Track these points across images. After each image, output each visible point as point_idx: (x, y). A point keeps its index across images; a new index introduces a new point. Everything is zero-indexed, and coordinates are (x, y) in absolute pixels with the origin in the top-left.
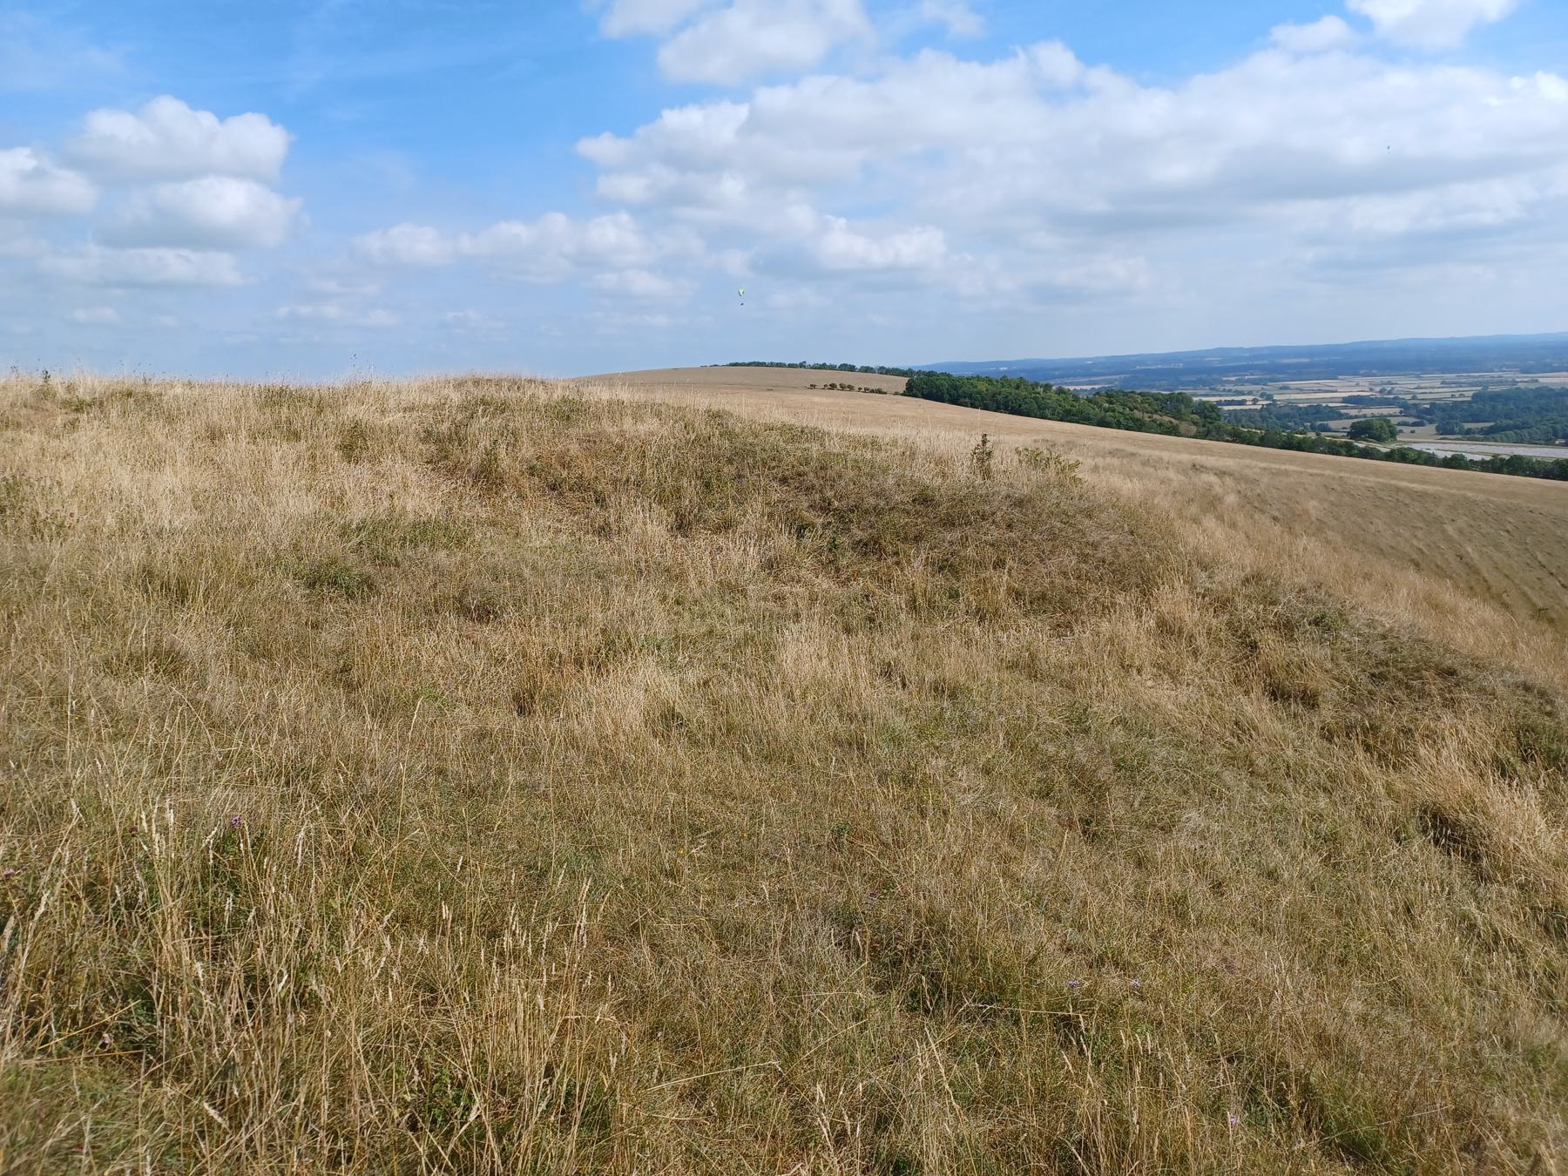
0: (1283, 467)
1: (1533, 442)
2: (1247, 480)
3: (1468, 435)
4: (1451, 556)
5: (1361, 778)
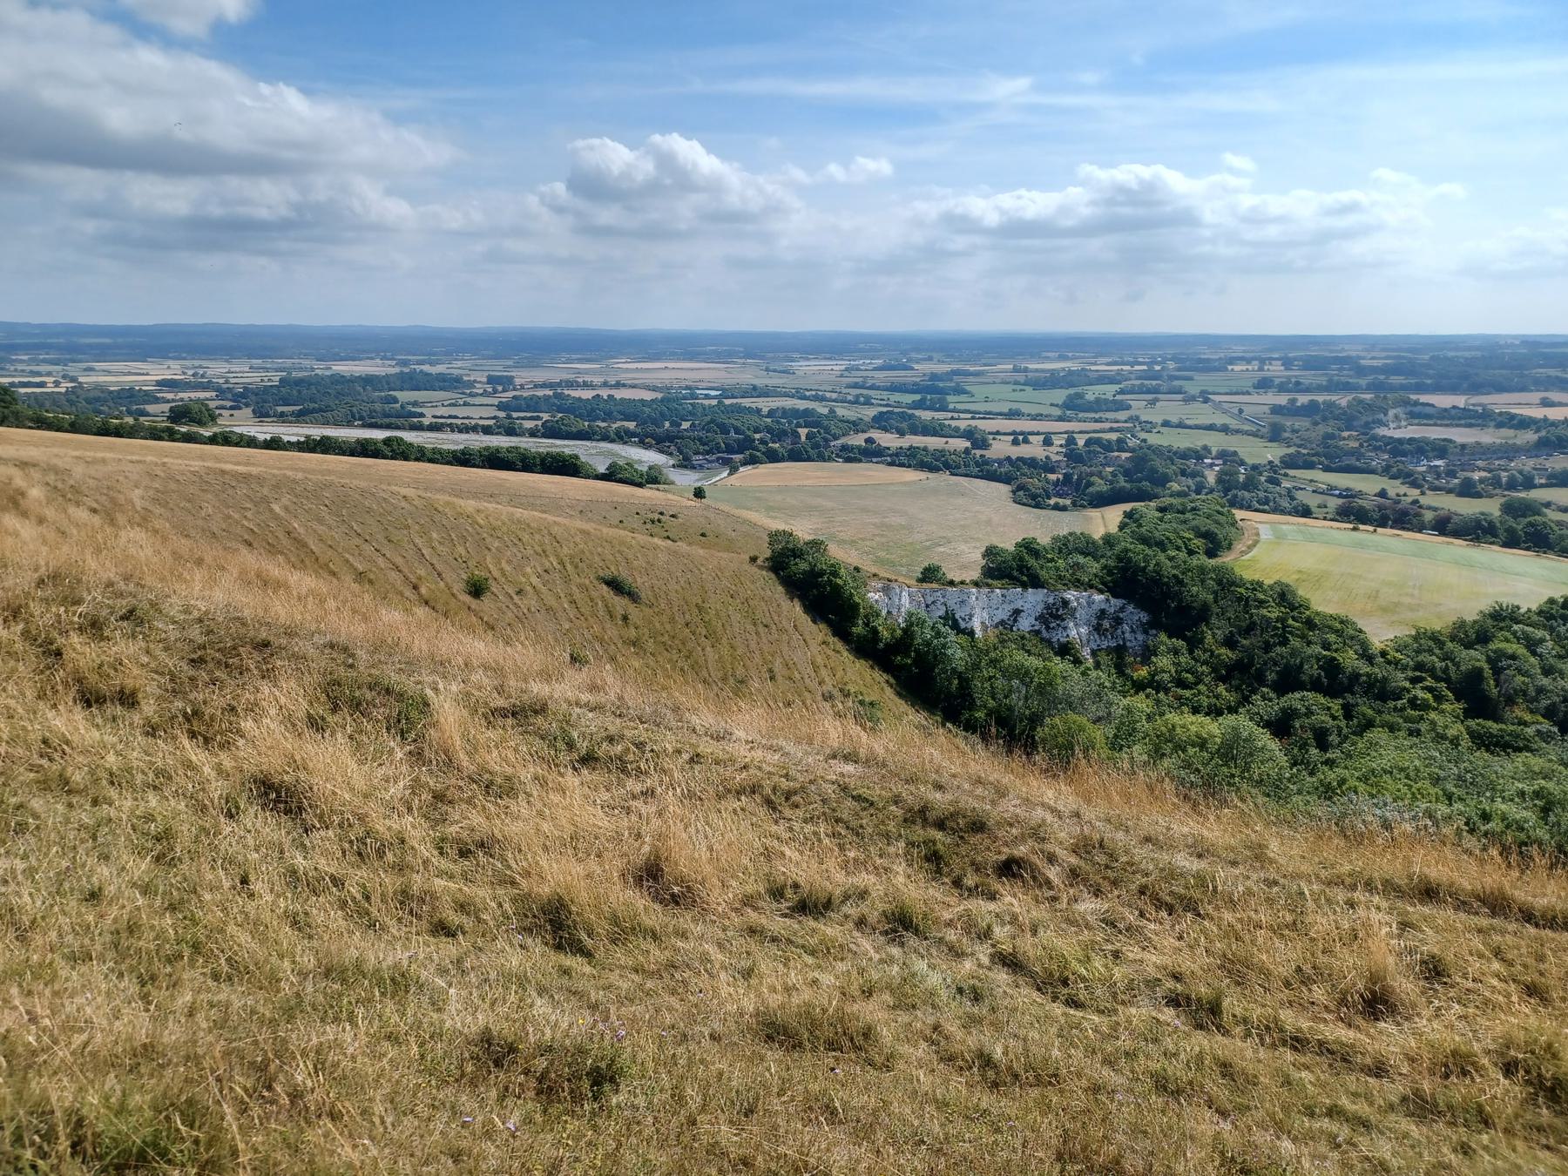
0: (100, 455)
1: (337, 424)
2: (56, 470)
3: (282, 418)
4: (281, 535)
5: (189, 765)
